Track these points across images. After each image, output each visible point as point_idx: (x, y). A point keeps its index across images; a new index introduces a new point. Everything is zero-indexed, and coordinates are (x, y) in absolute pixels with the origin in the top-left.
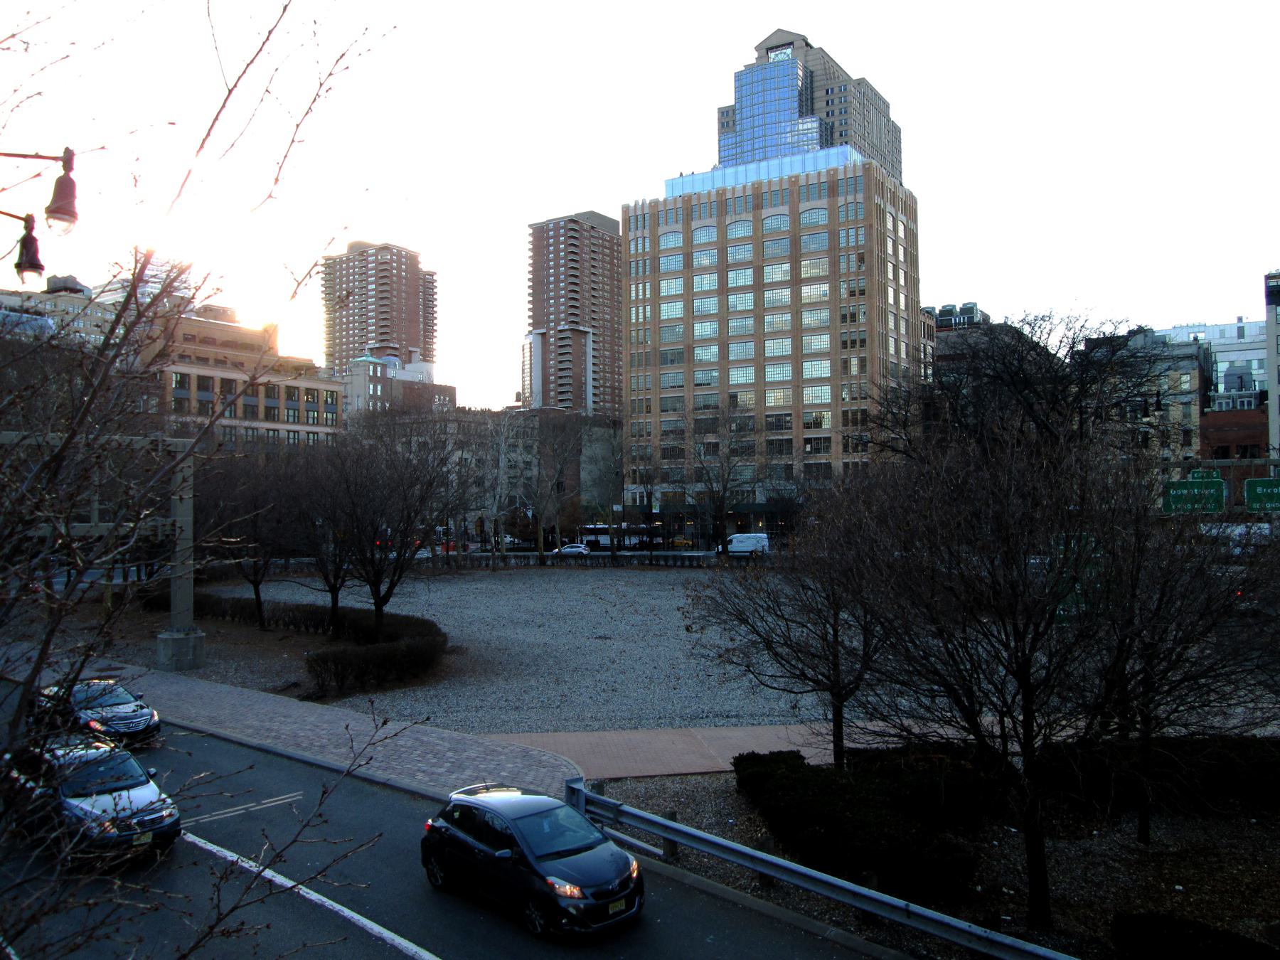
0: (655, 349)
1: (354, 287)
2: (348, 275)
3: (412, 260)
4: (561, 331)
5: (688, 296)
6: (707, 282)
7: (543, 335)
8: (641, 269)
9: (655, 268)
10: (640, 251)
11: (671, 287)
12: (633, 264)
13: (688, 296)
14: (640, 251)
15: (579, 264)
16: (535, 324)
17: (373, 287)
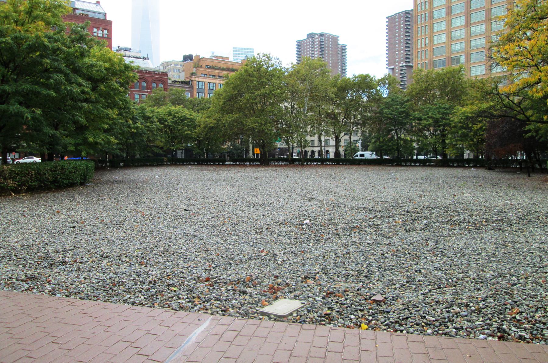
0: (430, 60)
1: (309, 57)
2: (307, 49)
3: (335, 39)
4: (401, 67)
5: (449, 31)
6: (460, 22)
7: (393, 69)
8: (423, 20)
9: (431, 18)
10: (423, 9)
11: (440, 27)
12: (419, 17)
13: (449, 31)
14: (423, 9)
15: (404, 29)
16: (389, 65)
17: (317, 53)
